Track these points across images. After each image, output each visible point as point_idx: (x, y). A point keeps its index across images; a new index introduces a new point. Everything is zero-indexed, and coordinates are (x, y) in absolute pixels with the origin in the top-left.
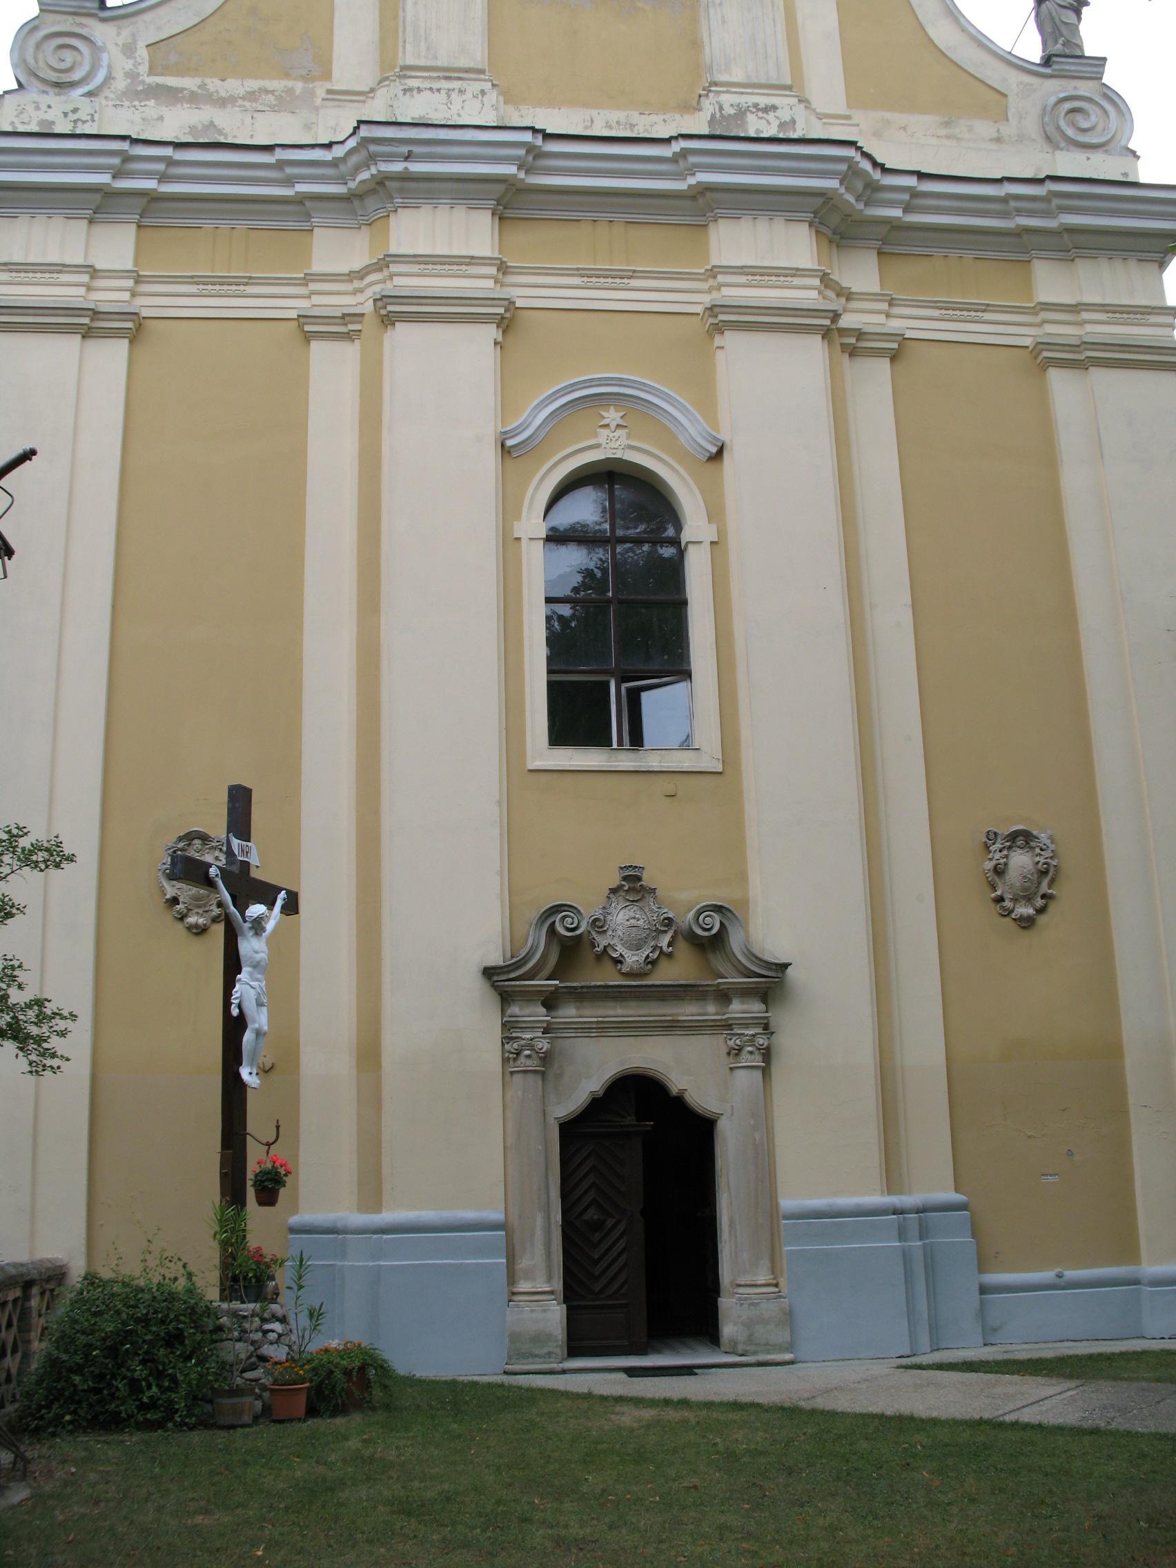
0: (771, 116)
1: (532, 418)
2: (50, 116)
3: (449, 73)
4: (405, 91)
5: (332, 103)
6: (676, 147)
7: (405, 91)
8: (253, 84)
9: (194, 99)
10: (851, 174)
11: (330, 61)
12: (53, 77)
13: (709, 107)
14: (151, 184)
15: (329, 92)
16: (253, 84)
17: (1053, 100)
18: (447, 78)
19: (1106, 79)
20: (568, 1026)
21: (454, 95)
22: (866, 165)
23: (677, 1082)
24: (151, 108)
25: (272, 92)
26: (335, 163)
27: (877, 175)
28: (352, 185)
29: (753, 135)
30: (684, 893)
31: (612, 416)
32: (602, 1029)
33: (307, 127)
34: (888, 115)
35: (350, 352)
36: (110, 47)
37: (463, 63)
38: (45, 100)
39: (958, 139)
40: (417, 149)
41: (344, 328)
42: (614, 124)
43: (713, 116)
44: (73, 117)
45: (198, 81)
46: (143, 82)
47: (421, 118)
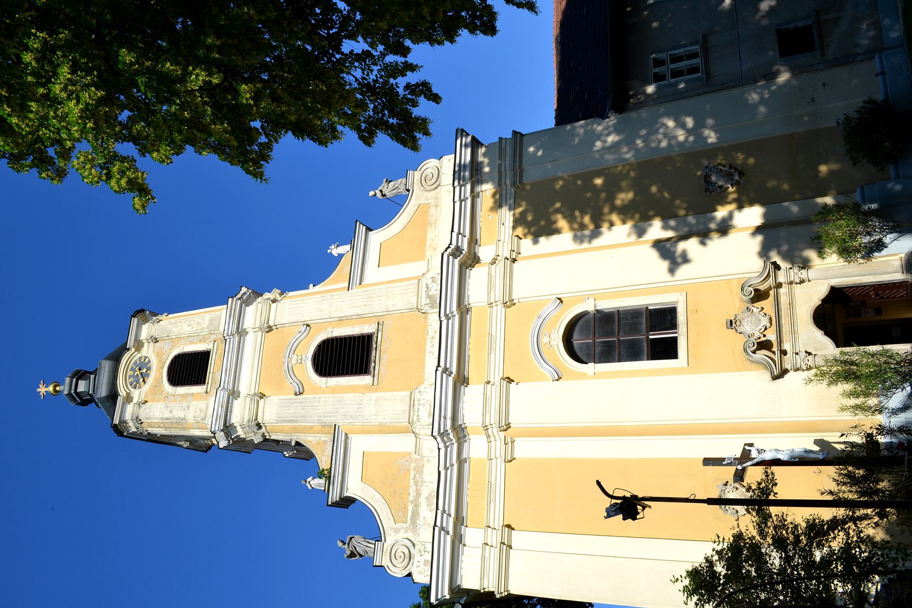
0: (430, 286)
1: (547, 371)
2: (422, 561)
3: (412, 405)
6: (443, 318)
8: (412, 482)
9: (417, 505)
12: (407, 560)
14: (451, 520)
20: (793, 346)
22: (449, 250)
23: (816, 301)
24: (420, 521)
26: (446, 447)
27: (452, 247)
28: (454, 441)
30: (735, 304)
31: (544, 340)
32: (793, 332)
35: (518, 442)
36: (395, 538)
37: (408, 400)
38: (416, 563)
40: (443, 414)
41: (509, 443)
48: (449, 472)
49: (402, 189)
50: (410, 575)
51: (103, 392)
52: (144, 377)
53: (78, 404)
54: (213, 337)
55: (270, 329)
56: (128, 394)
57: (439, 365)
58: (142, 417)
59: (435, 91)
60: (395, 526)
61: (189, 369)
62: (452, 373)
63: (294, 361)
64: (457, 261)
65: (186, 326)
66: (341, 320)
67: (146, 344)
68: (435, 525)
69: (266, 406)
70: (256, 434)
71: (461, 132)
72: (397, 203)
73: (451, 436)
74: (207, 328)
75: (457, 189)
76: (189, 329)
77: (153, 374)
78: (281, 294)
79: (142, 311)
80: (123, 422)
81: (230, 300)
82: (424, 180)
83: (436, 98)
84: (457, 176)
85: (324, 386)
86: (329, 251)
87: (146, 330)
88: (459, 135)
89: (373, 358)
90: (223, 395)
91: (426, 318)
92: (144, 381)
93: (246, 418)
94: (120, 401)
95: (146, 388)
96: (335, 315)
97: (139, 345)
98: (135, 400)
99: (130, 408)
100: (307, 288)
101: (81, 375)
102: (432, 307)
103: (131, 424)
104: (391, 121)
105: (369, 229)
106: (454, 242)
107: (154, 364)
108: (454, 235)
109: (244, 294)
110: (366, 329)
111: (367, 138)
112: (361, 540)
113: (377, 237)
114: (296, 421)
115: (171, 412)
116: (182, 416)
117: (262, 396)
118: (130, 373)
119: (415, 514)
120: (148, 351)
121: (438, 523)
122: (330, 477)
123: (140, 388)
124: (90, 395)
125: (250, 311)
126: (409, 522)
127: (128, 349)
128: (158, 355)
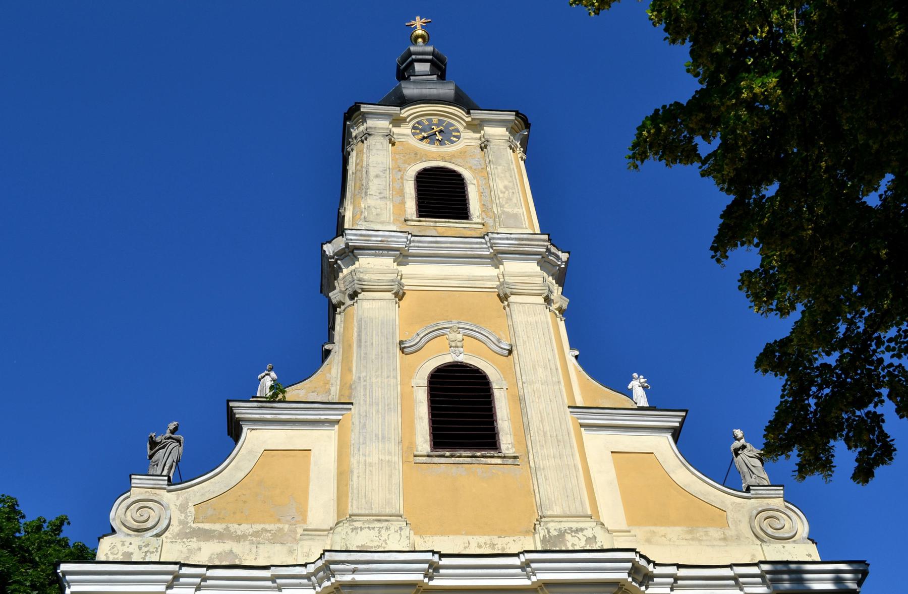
0: (580, 535)
2: (131, 549)
3: (380, 517)
4: (353, 530)
5: (306, 537)
7: (353, 530)
8: (258, 527)
9: (221, 537)
10: (635, 571)
11: (306, 511)
13: (541, 531)
15: (305, 530)
16: (258, 527)
17: (755, 512)
18: (379, 521)
19: (789, 334)
21: (383, 531)
22: (643, 562)
24: (194, 543)
25: (270, 531)
26: (308, 577)
27: (650, 567)
29: (571, 548)
33: (291, 552)
34: (653, 528)
36: (172, 507)
37: (388, 511)
39: (700, 541)
42: (483, 545)
43: (544, 536)
44: (144, 549)
45: (224, 526)
46: (190, 527)
47: (362, 546)
48: (269, 583)
49: (750, 480)
50: (113, 531)
51: (409, 90)
52: (430, 138)
53: (398, 67)
54: (490, 222)
55: (503, 298)
56: (404, 120)
57: (442, 556)
58: (371, 140)
59: (879, 471)
60: (191, 504)
61: (441, 194)
62: (431, 579)
63: (452, 336)
64: (624, 576)
65: (506, 183)
66: (519, 401)
67: (478, 135)
68: (182, 565)
69: (383, 303)
70: (343, 293)
71: (862, 571)
72: (728, 477)
73: (327, 584)
74: (503, 212)
75: (755, 570)
76: (501, 186)
77: (434, 149)
78: (560, 310)
79: (527, 126)
80: (364, 117)
81: (546, 237)
82: (769, 514)
83: (863, 473)
84: (780, 567)
85: (413, 382)
86: (635, 375)
87: (498, 133)
88: (855, 567)
89: (458, 453)
90: (399, 241)
91: (527, 533)
92: (424, 138)
93: (366, 277)
94: (394, 110)
95: (414, 142)
96: (528, 391)
97: (475, 126)
98: (396, 130)
99: (384, 124)
100: (572, 347)
101: (439, 67)
102: (544, 541)
103: (362, 128)
104: (812, 401)
105: (676, 434)
106: (658, 570)
107: (449, 149)
108: (672, 570)
109: (558, 257)
110: (507, 442)
111: (772, 358)
112: (174, 457)
113: (663, 445)
114: (359, 346)
115: (377, 176)
116: (370, 192)
117: (399, 296)
118: (435, 119)
119: (207, 535)
120: (468, 139)
121: (185, 570)
122: (274, 402)
123: (414, 134)
124: (409, 76)
125: (532, 267)
126: (195, 525)
127: (468, 113)
128: (463, 153)
